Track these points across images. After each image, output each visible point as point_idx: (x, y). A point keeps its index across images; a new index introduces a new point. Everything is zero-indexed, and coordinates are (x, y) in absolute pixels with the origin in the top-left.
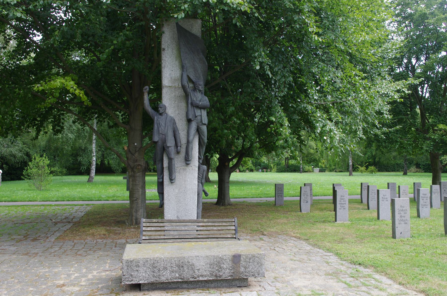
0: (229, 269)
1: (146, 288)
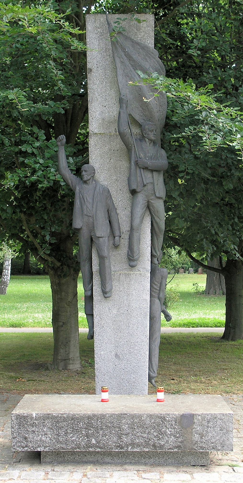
0: (174, 436)
1: (48, 460)
